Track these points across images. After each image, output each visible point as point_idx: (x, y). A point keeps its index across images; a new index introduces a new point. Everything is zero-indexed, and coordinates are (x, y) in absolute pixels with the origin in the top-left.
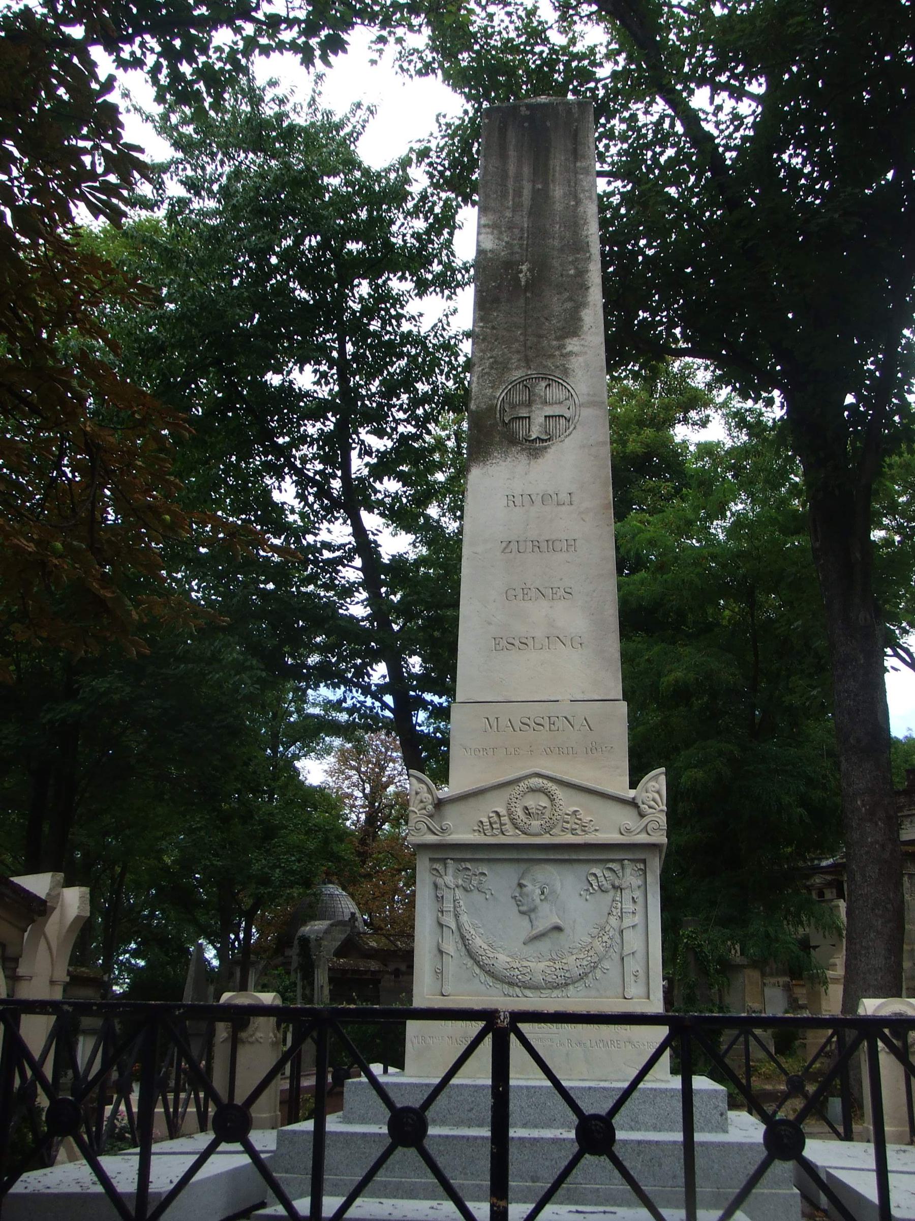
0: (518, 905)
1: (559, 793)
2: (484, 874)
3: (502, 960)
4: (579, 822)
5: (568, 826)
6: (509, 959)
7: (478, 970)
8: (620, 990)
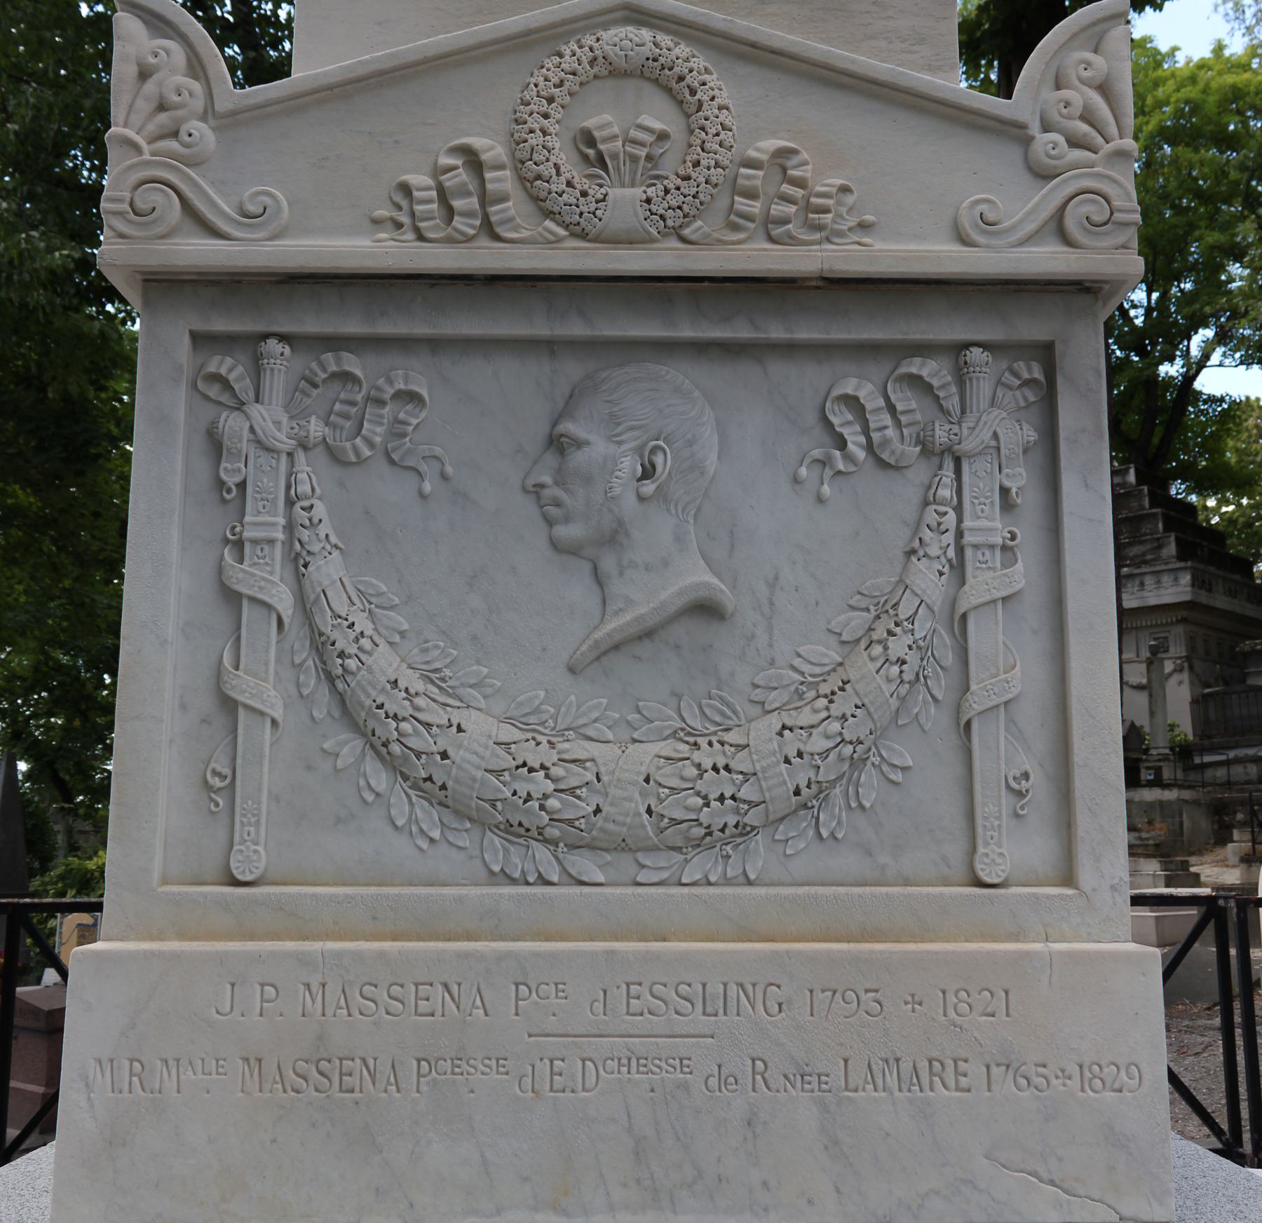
0: (550, 522)
1: (720, 85)
2: (412, 397)
3: (478, 737)
4: (798, 193)
5: (755, 207)
6: (508, 733)
7: (380, 779)
8: (955, 851)
